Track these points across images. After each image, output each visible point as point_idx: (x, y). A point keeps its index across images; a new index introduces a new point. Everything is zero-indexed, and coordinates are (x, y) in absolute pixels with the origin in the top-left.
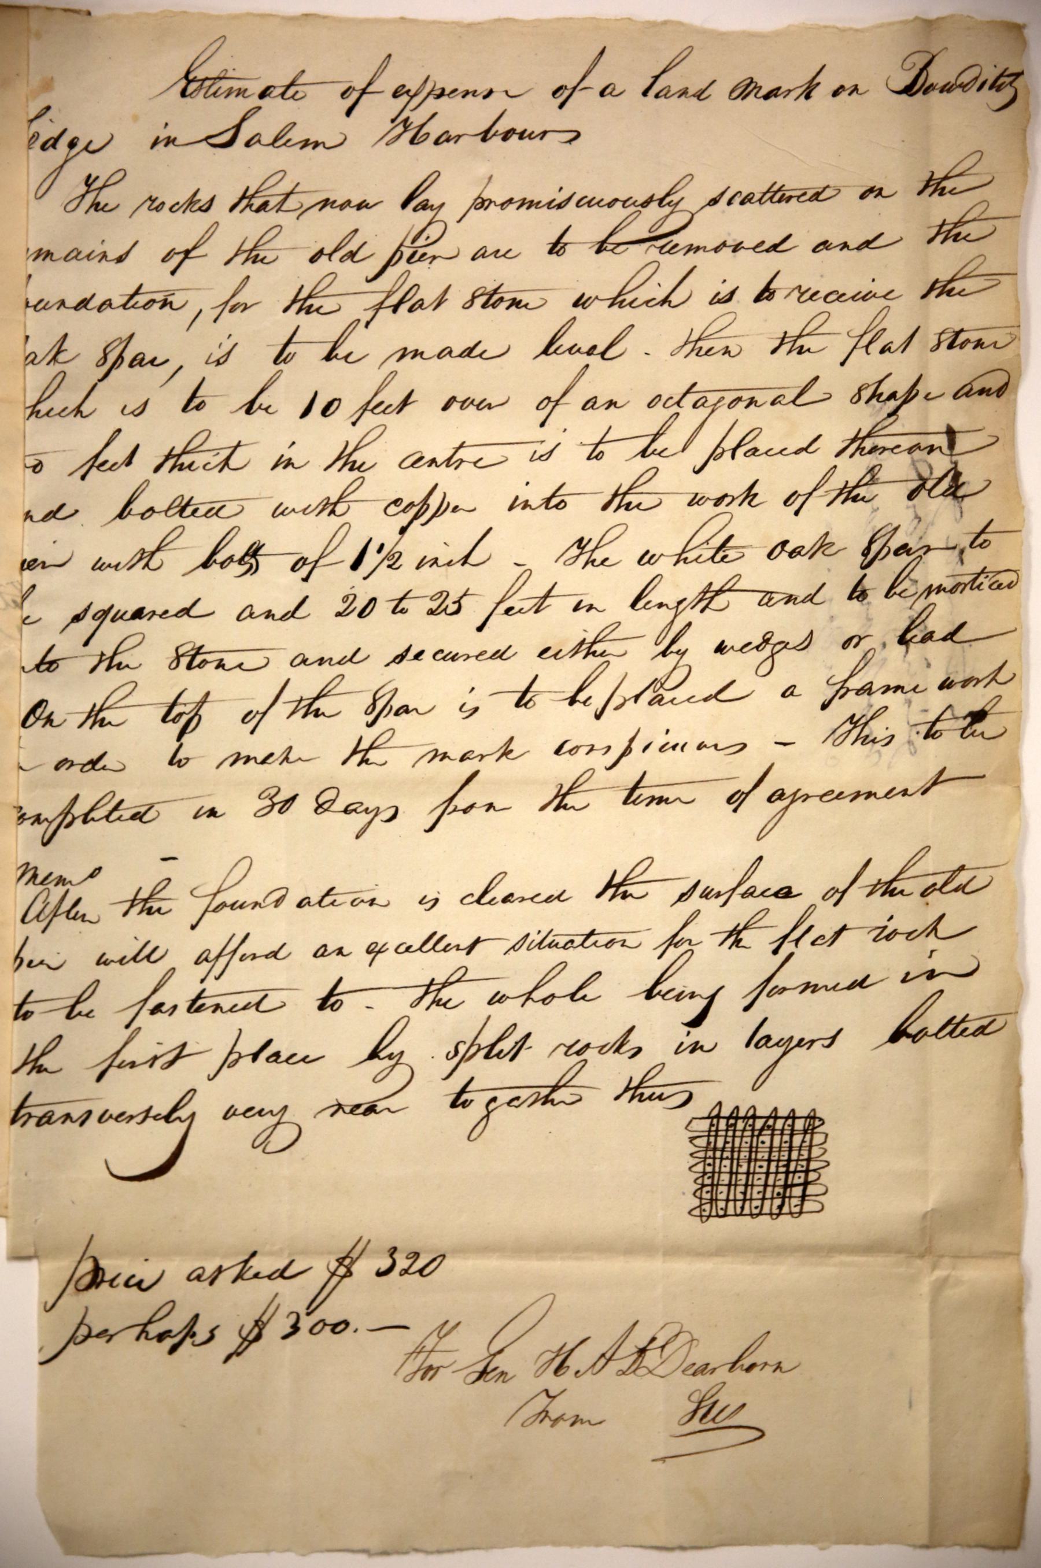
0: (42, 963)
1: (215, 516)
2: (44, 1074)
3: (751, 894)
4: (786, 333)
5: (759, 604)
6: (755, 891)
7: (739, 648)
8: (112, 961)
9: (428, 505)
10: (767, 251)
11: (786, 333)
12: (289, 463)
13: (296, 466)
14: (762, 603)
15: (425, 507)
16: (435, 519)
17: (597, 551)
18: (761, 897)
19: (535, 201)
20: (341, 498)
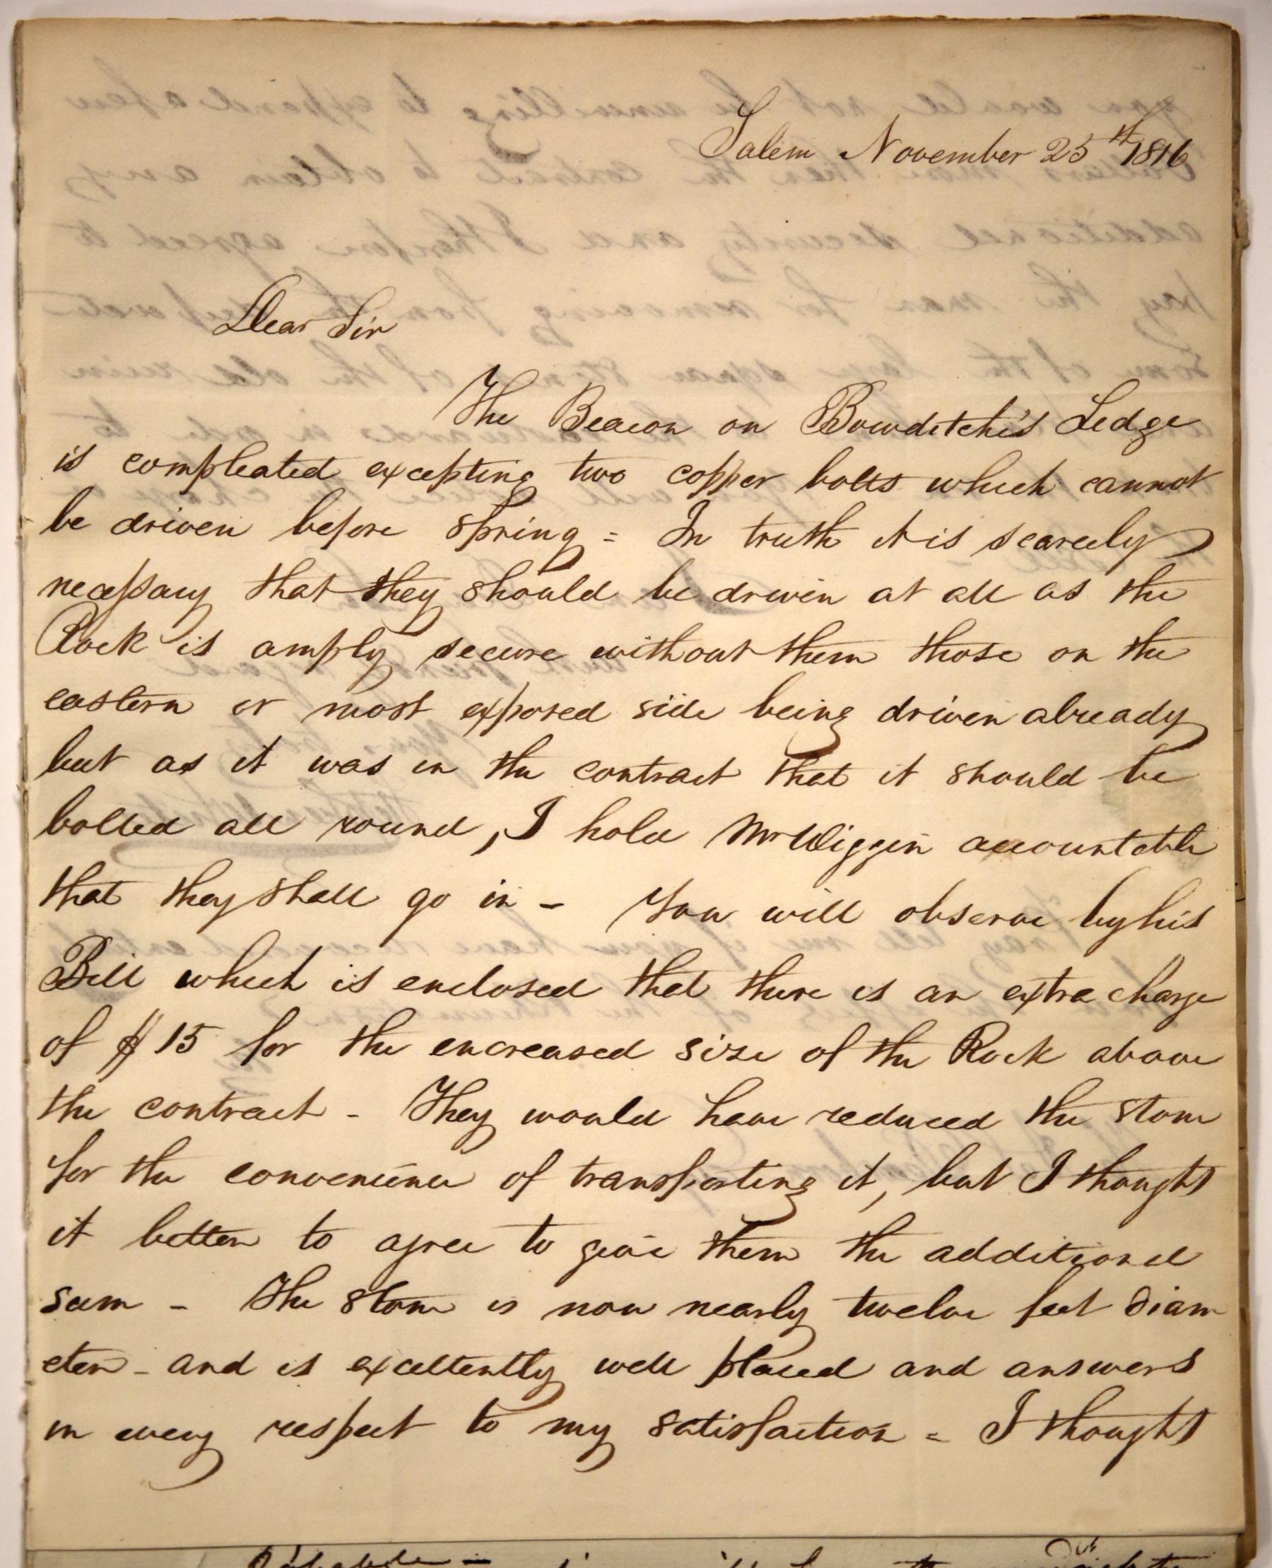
0: (421, 434)
1: (1129, 1058)
2: (783, 1260)
3: (681, 778)
4: (1057, 1412)
5: (170, 1370)
6: (687, 774)
7: (593, 1051)
8: (785, 1257)
9: (409, 905)
10: (280, 331)
11: (1057, 1412)
12: (68, 1431)
13: (78, 1435)
14: (174, 1369)
15: (415, 902)
16: (716, 1380)
17: (462, 1098)
18: (696, 718)
19: (544, 530)
20: (76, 1039)
